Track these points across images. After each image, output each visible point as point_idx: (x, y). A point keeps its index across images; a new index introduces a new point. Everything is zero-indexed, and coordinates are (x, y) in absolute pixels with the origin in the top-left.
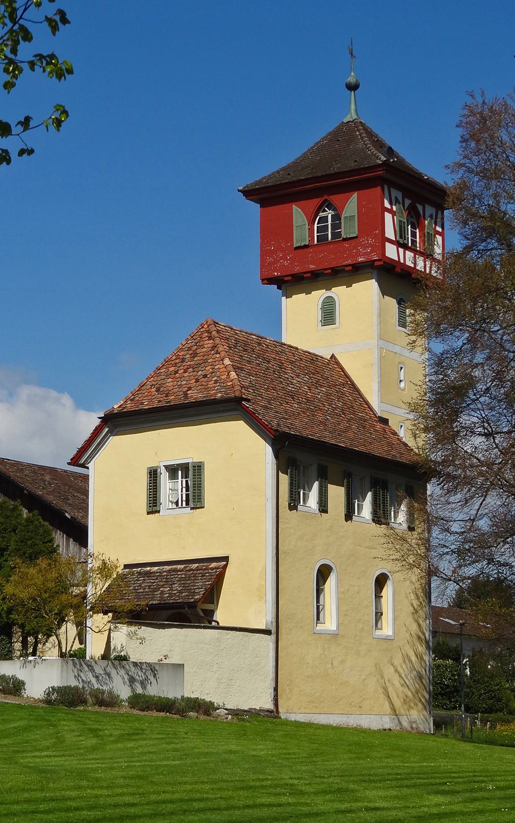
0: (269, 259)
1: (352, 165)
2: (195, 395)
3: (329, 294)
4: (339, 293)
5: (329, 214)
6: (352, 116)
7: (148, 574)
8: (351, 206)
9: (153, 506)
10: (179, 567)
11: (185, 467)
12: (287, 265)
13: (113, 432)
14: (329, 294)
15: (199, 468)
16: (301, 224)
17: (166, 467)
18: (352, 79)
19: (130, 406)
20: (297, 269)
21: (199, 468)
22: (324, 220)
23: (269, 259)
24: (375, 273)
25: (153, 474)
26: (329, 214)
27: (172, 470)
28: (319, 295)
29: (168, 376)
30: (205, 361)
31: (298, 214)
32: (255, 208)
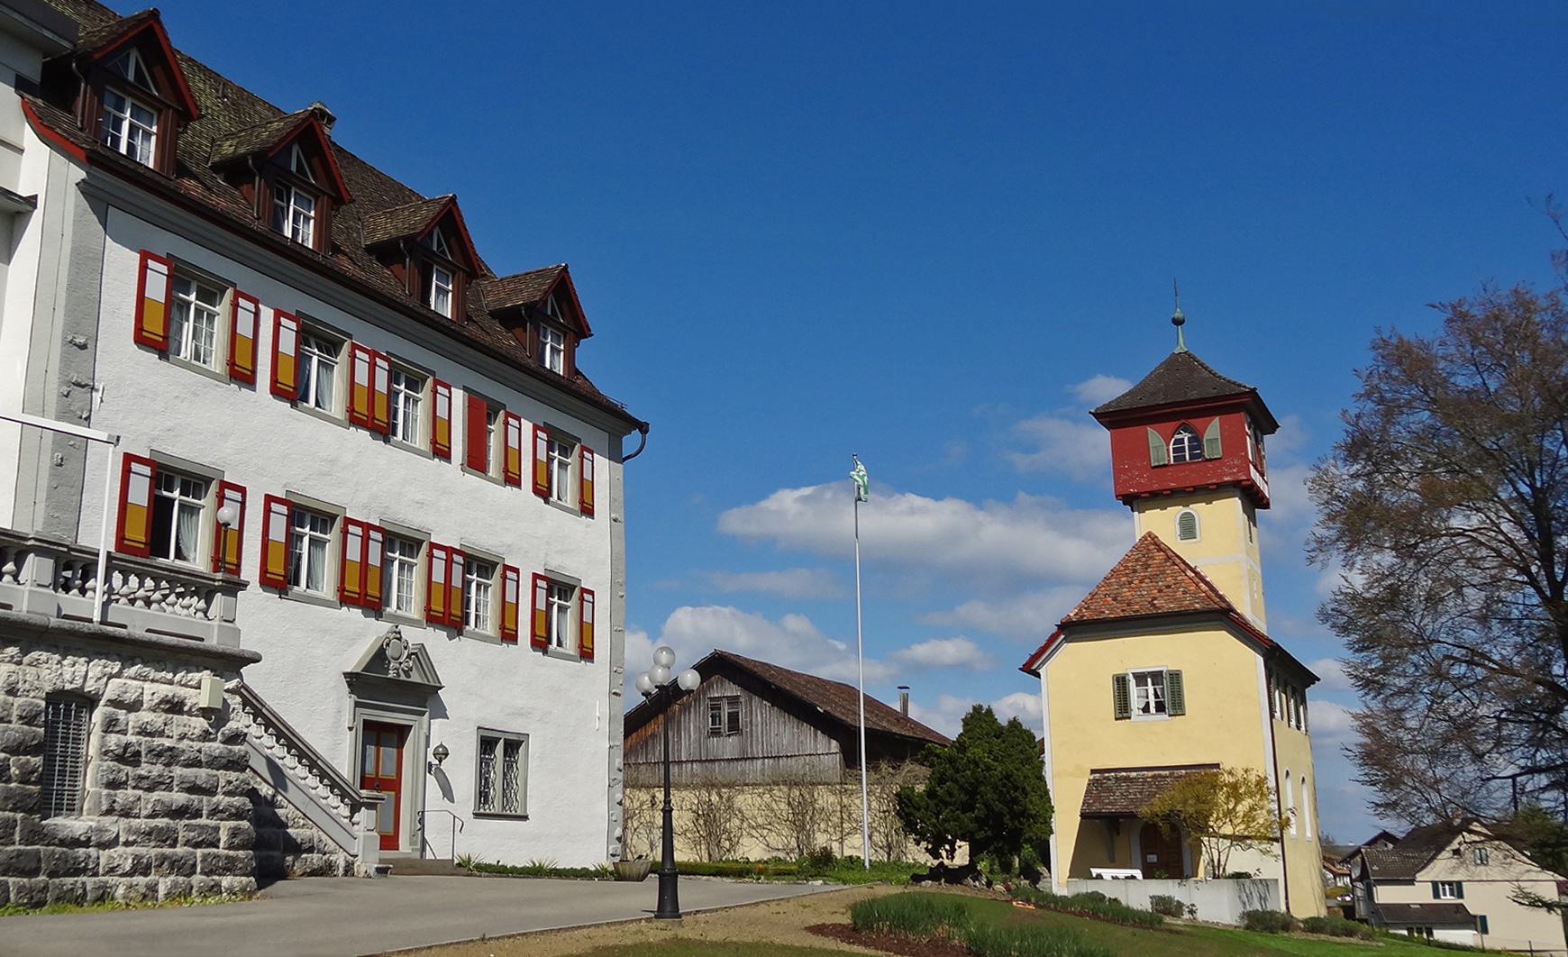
0: (1123, 477)
1: (1214, 393)
2: (1165, 605)
3: (1187, 510)
4: (1198, 509)
5: (1186, 436)
6: (1181, 348)
7: (1126, 779)
8: (1213, 430)
9: (1123, 710)
10: (1134, 774)
11: (1157, 677)
12: (1143, 482)
13: (1067, 640)
14: (1187, 510)
15: (1176, 677)
16: (1160, 445)
17: (1136, 676)
18: (1178, 315)
19: (1087, 615)
20: (1155, 487)
21: (1176, 677)
22: (1182, 441)
23: (1123, 477)
24: (1238, 492)
25: (1121, 682)
26: (1186, 436)
27: (1141, 679)
28: (1176, 511)
29: (1122, 586)
30: (1163, 572)
31: (1153, 436)
32: (1104, 435)
